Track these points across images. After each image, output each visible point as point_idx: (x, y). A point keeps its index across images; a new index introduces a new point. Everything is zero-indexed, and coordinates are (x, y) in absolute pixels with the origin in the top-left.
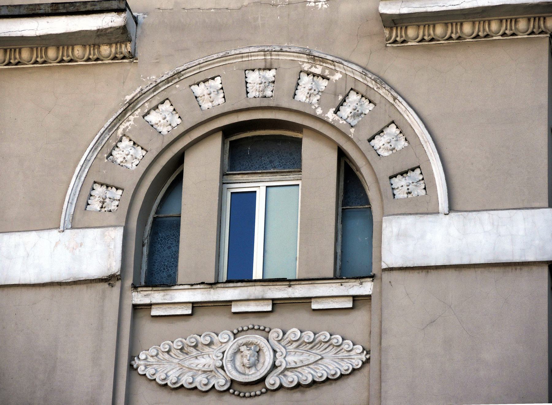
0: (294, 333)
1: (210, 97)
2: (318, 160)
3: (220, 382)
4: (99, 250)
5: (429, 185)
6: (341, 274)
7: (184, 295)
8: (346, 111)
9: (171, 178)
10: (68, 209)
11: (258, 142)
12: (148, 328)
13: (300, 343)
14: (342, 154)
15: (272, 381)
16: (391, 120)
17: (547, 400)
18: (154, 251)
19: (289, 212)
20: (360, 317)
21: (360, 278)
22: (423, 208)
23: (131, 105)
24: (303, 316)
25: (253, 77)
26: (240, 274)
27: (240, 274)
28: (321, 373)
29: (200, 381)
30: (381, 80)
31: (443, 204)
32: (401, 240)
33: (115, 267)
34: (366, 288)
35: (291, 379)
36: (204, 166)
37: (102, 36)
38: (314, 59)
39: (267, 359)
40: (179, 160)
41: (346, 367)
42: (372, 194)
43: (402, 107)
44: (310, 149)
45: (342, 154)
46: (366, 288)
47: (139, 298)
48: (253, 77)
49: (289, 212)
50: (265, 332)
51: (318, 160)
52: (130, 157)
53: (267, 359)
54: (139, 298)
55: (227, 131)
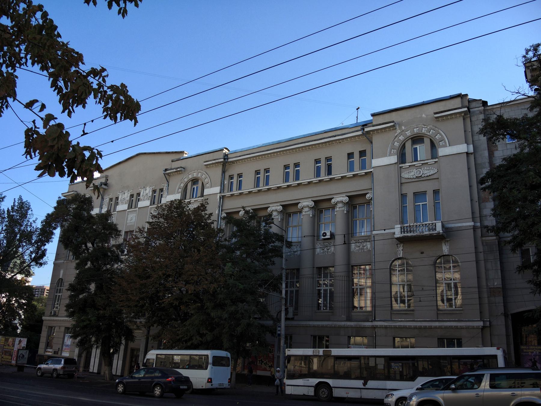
0: (426, 168)
1: (408, 133)
2: (427, 141)
3: (415, 177)
4: (393, 159)
5: (445, 143)
6: (432, 158)
7: (407, 164)
8: (431, 133)
9: (403, 147)
10: (388, 154)
11: (417, 139)
12: (402, 170)
13: (427, 170)
14: (431, 139)
15: (423, 176)
16: (392, 338)
17: (437, 345)
18: (402, 158)
19: (423, 150)
20: (436, 164)
21: (435, 158)
22: (445, 146)
23: (396, 136)
24: (426, 165)
25: (415, 129)
26: (416, 160)
27: (416, 160)
28: (430, 174)
29: (411, 177)
30: (436, 127)
31: (448, 145)
32: (442, 152)
33: (396, 161)
34: (437, 160)
35: (426, 175)
36: (408, 145)
37: (391, 127)
38: (425, 125)
39: (422, 173)
40: (405, 144)
41: (434, 172)
42: (436, 145)
43: (440, 131)
44: (425, 139)
45: (431, 139)
46: (437, 160)
47: (401, 166)
48: (415, 129)
49: (423, 150)
50: (421, 169)
51: (427, 141)
52: (397, 144)
53: (422, 173)
54: (401, 166)
55: (412, 138)
